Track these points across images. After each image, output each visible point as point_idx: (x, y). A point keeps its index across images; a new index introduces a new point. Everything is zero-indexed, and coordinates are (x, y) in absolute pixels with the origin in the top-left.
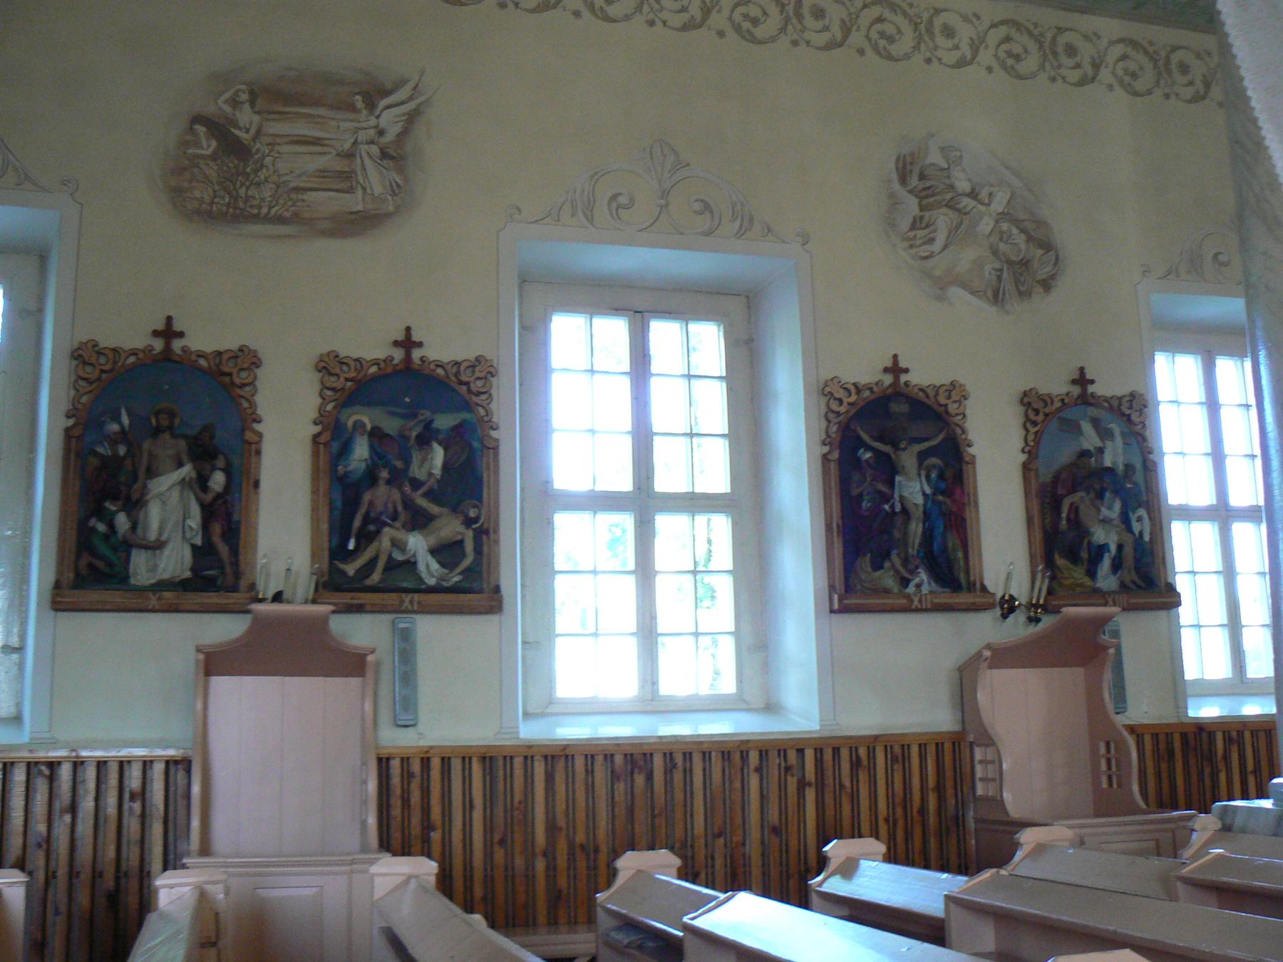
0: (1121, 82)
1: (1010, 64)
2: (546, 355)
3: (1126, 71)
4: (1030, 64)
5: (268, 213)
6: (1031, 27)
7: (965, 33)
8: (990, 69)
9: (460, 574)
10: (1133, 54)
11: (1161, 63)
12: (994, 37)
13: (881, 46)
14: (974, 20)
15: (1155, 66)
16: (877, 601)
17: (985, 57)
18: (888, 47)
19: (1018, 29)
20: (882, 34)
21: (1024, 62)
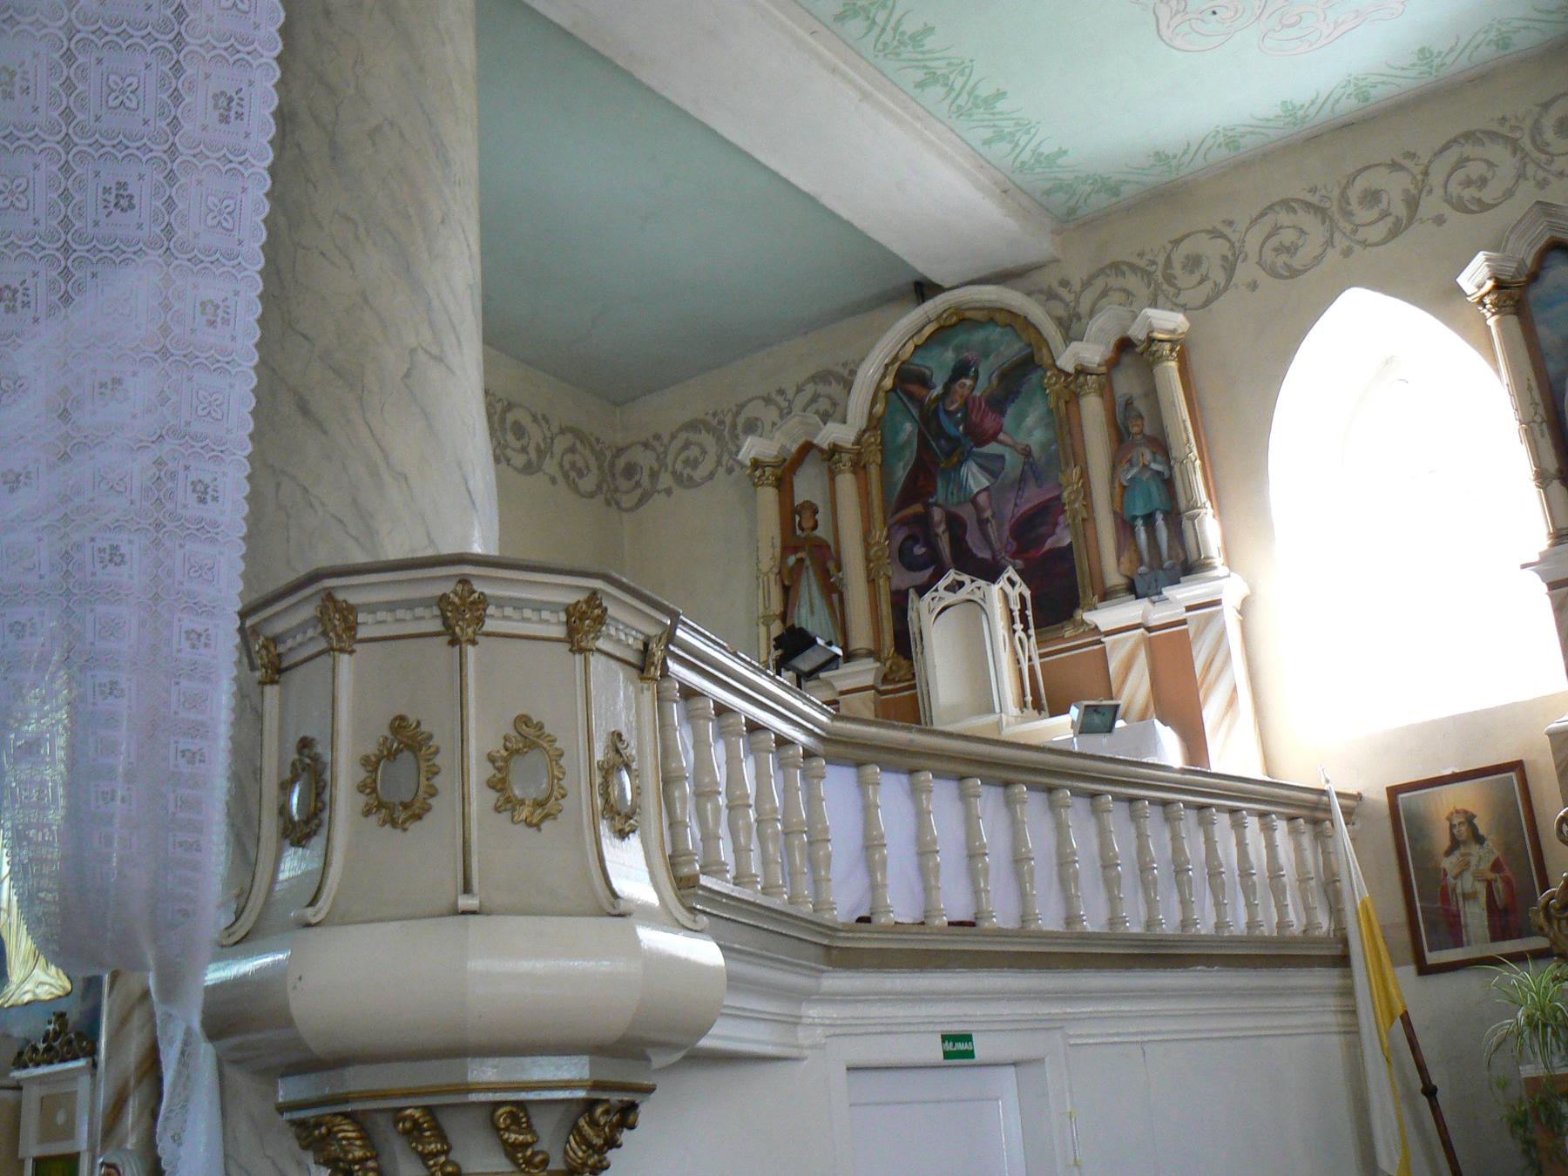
0: (566, 476)
1: (571, 475)
2: (937, 967)
3: (573, 465)
4: (587, 484)
5: (357, 1139)
6: (594, 443)
7: (535, 433)
8: (553, 480)
9: (902, 448)
10: (579, 446)
11: (606, 464)
12: (561, 443)
13: (571, 478)
14: (543, 422)
15: (600, 467)
16: (1110, 1009)
17: (550, 466)
18: (577, 480)
19: (582, 441)
20: (573, 465)
21: (585, 479)
